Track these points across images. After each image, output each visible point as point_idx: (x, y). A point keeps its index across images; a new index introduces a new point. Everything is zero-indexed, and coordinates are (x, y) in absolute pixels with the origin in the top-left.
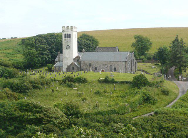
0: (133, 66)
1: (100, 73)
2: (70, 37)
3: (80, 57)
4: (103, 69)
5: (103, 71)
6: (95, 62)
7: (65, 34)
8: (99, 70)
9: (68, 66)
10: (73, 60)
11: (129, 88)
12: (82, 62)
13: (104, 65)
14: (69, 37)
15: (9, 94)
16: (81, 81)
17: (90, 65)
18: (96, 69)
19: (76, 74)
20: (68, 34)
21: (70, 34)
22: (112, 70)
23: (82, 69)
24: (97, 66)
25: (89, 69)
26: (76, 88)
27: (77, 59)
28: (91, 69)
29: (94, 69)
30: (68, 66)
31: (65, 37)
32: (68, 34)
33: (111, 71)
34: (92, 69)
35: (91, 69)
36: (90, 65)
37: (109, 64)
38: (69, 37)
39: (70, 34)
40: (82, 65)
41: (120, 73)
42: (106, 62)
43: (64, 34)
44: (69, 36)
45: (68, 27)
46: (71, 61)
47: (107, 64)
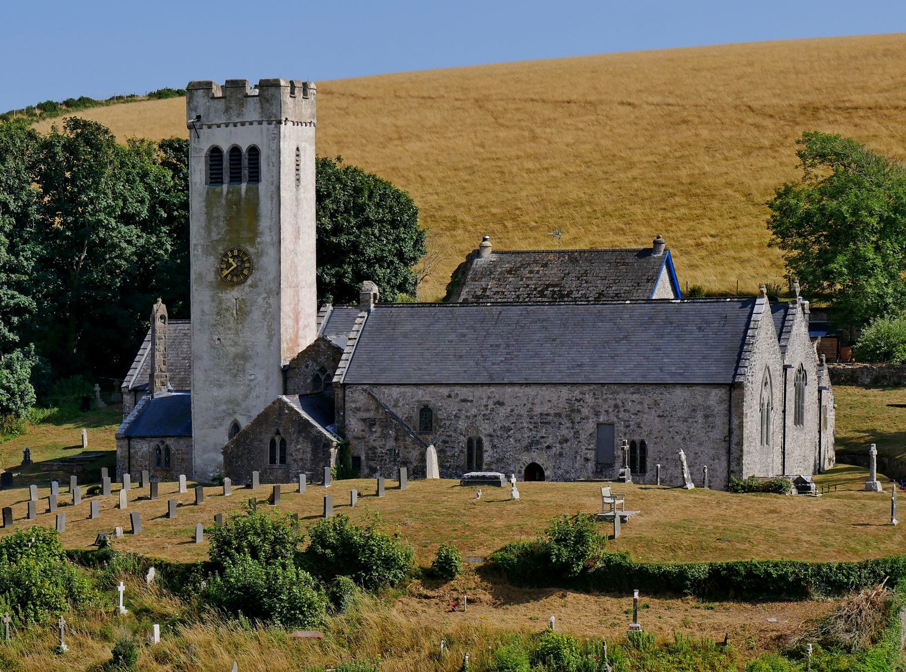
0: (799, 419)
1: (515, 488)
2: (255, 177)
3: (338, 351)
4: (540, 458)
5: (534, 473)
6: (464, 392)
7: (215, 152)
8: (500, 463)
9: (236, 426)
10: (277, 379)
11: (384, 629)
12: (356, 399)
13: (544, 420)
14: (245, 172)
15: (768, 566)
16: (342, 560)
17: (427, 415)
18: (474, 454)
19: (308, 504)
20: (235, 150)
21: (254, 151)
22: (611, 466)
23: (357, 459)
24: (485, 428)
25: (414, 454)
26: (210, 203)
27: (314, 375)
28: (432, 454)
29: (463, 458)
30: (236, 426)
31: (214, 178)
32: (235, 150)
33: (603, 470)
34: (440, 452)
35: (432, 454)
36: (427, 415)
37: (585, 411)
38: (245, 172)
39: (254, 151)
40: (354, 425)
41: (683, 486)
42: (565, 392)
43: (206, 147)
44: (245, 162)
45: (235, 86)
46: (262, 392)
47: (573, 411)
